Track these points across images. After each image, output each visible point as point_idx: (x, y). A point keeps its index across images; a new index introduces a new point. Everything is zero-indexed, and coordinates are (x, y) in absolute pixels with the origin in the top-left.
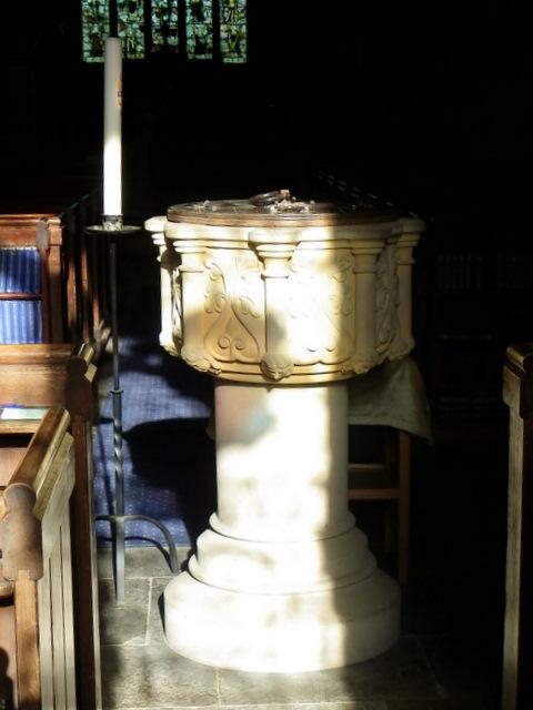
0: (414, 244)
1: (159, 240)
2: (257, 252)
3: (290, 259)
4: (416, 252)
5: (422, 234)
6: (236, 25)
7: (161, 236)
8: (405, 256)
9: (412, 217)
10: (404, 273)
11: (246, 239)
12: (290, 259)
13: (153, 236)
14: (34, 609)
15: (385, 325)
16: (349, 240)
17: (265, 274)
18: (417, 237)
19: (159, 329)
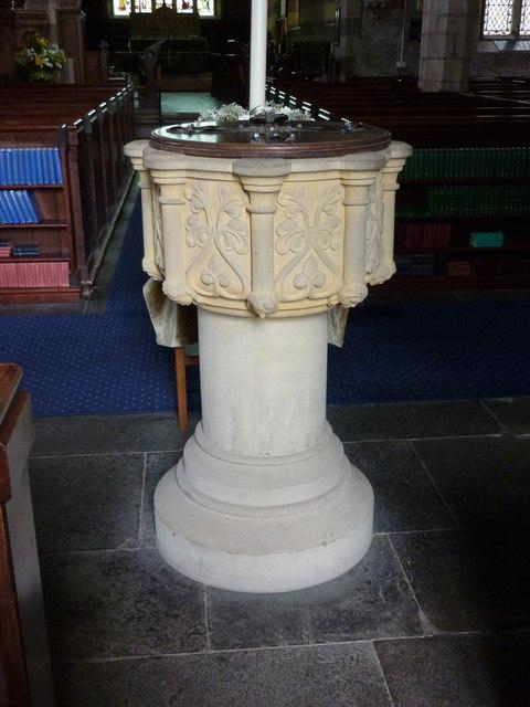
0: (401, 169)
1: (138, 165)
2: (242, 185)
3: (278, 192)
4: (401, 178)
5: (408, 160)
6: (465, 5)
7: (140, 162)
8: (392, 183)
9: (335, 326)
10: (389, 200)
11: (231, 171)
12: (278, 192)
13: (133, 161)
14: (12, 535)
15: (371, 256)
16: (341, 171)
17: (251, 208)
18: (403, 163)
19: (141, 255)
